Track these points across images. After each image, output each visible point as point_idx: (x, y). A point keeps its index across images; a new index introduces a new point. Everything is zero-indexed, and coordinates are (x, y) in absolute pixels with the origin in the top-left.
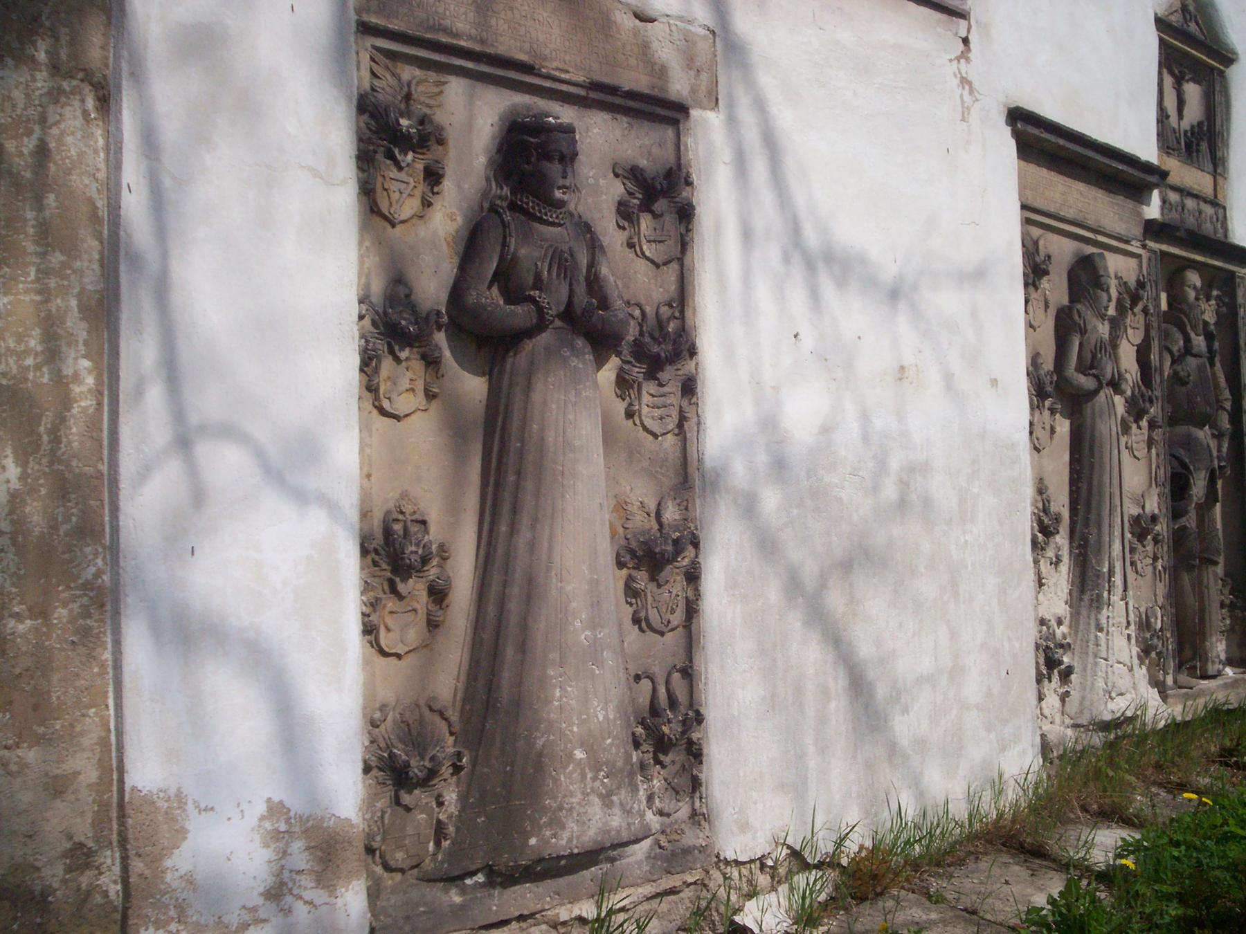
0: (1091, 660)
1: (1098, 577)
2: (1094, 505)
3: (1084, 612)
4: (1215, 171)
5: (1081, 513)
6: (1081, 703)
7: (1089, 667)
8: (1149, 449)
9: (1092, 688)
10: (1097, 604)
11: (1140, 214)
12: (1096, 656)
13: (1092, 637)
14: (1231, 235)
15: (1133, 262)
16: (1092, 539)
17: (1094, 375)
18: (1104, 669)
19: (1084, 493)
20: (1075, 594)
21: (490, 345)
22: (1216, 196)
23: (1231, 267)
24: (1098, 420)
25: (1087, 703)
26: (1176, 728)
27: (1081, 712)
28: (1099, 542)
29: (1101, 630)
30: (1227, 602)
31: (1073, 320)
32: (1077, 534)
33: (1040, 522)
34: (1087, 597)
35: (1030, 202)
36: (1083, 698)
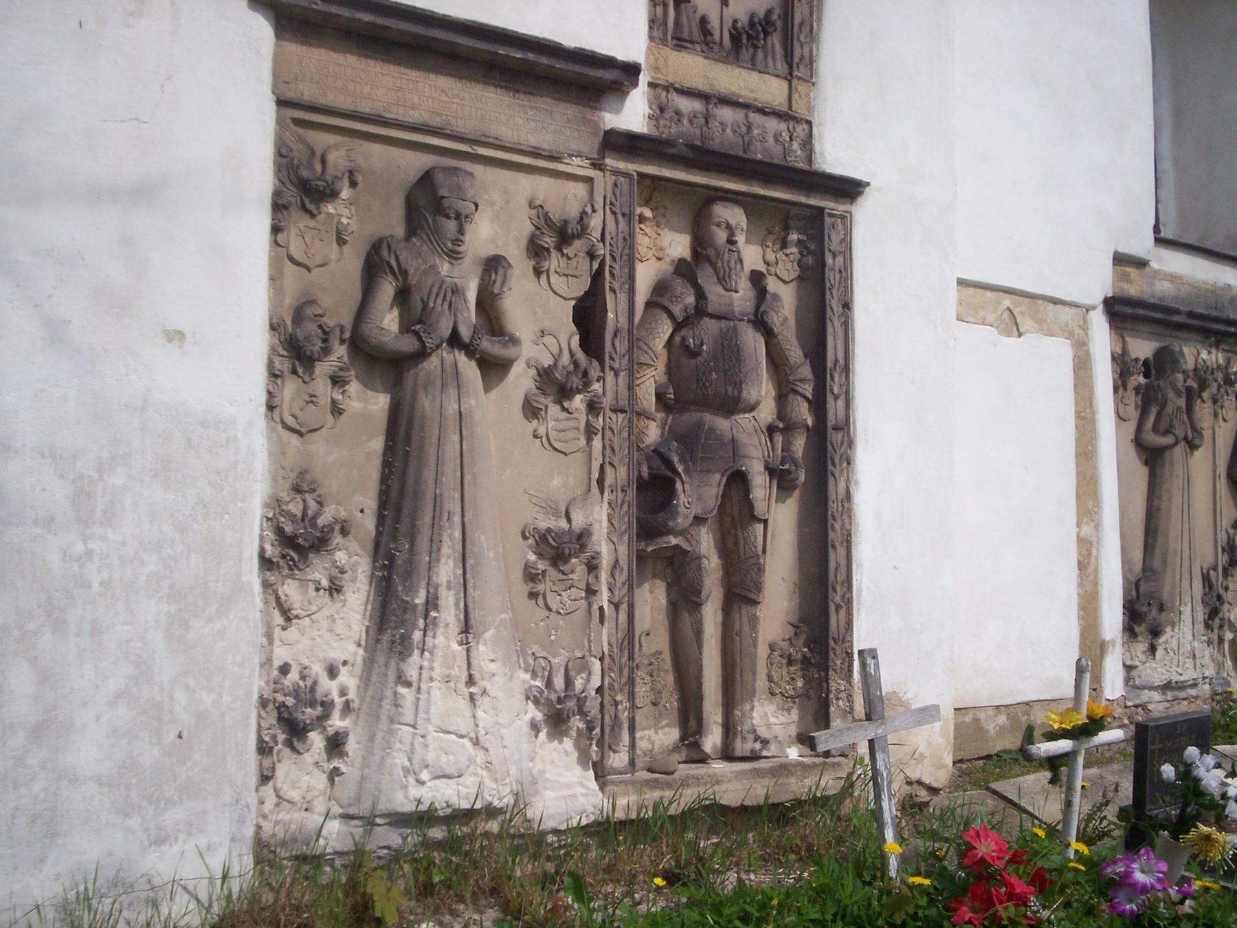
0: (384, 724)
1: (405, 610)
2: (405, 511)
3: (381, 659)
4: (791, 74)
5: (389, 522)
6: (361, 786)
7: (380, 735)
8: (589, 440)
9: (381, 764)
10: (402, 648)
11: (596, 125)
12: (392, 721)
13: (389, 693)
14: (817, 158)
15: (580, 189)
16: (400, 558)
17: (416, 333)
18: (407, 739)
19: (394, 493)
20: (371, 633)
21: (389, 367)
22: (790, 108)
23: (813, 202)
24: (421, 394)
25: (369, 786)
26: (603, 830)
27: (358, 798)
28: (411, 562)
29: (408, 684)
30: (799, 656)
31: (380, 257)
32: (382, 551)
33: (279, 531)
34: (386, 638)
35: (290, 95)
36: (363, 778)
